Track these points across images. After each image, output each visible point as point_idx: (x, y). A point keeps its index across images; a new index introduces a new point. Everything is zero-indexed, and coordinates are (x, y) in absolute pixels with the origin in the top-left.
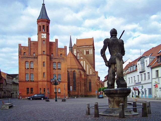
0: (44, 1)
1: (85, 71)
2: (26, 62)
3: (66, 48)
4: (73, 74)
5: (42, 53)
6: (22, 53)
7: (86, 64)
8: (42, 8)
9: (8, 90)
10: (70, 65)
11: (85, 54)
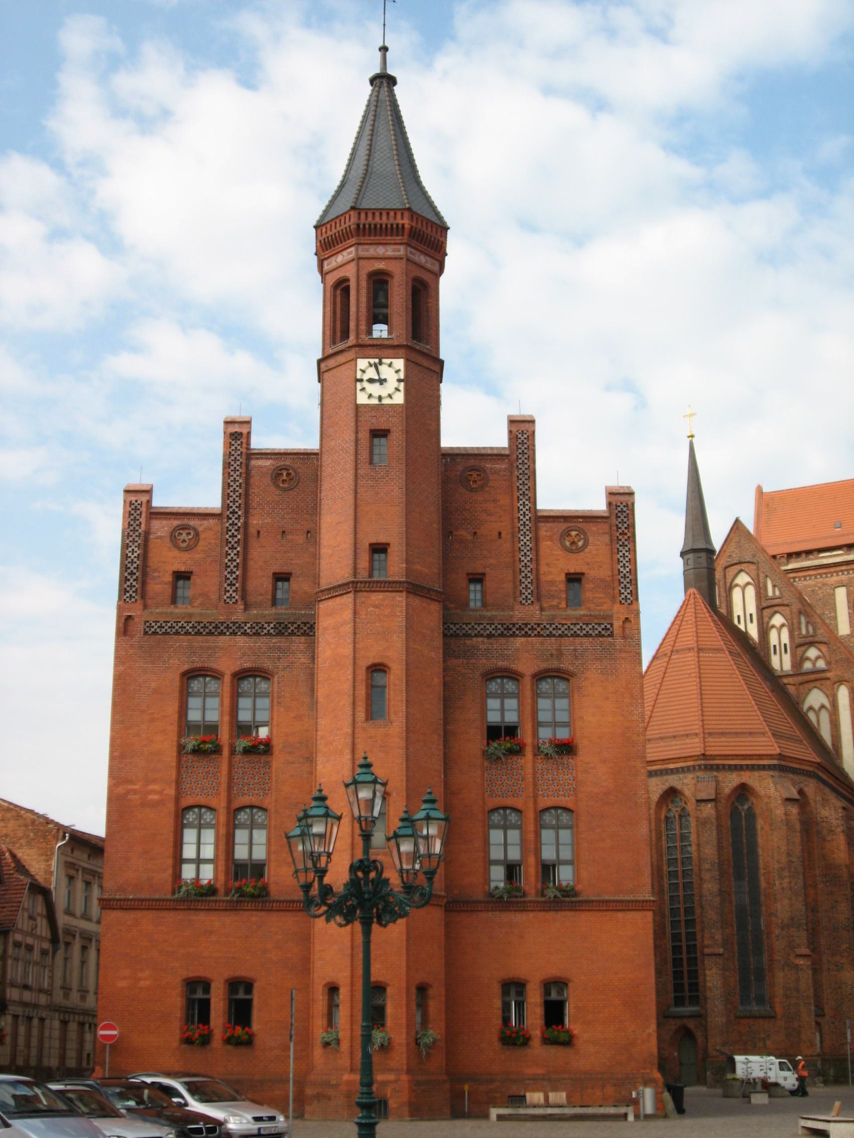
0: (384, 49)
2: (190, 675)
3: (621, 505)
4: (736, 830)
5: (364, 563)
6: (160, 585)
8: (367, 112)
10: (697, 728)
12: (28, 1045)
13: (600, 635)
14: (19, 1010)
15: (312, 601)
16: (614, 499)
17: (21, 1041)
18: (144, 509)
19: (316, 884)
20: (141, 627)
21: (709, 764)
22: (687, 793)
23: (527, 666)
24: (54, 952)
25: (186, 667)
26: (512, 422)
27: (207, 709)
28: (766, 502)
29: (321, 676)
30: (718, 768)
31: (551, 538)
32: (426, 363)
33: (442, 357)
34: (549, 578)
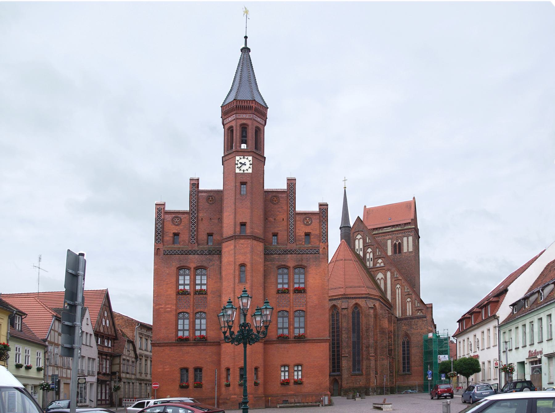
1: (389, 306)
2: (180, 268)
3: (324, 208)
7: (395, 281)
9: (143, 377)
11: (390, 253)
14: (126, 381)
15: (220, 243)
16: (322, 207)
17: (127, 390)
18: (162, 211)
19: (228, 331)
20: (162, 252)
21: (345, 297)
22: (339, 306)
23: (291, 264)
27: (185, 281)
28: (367, 212)
29: (223, 268)
31: (300, 221)
34: (299, 234)
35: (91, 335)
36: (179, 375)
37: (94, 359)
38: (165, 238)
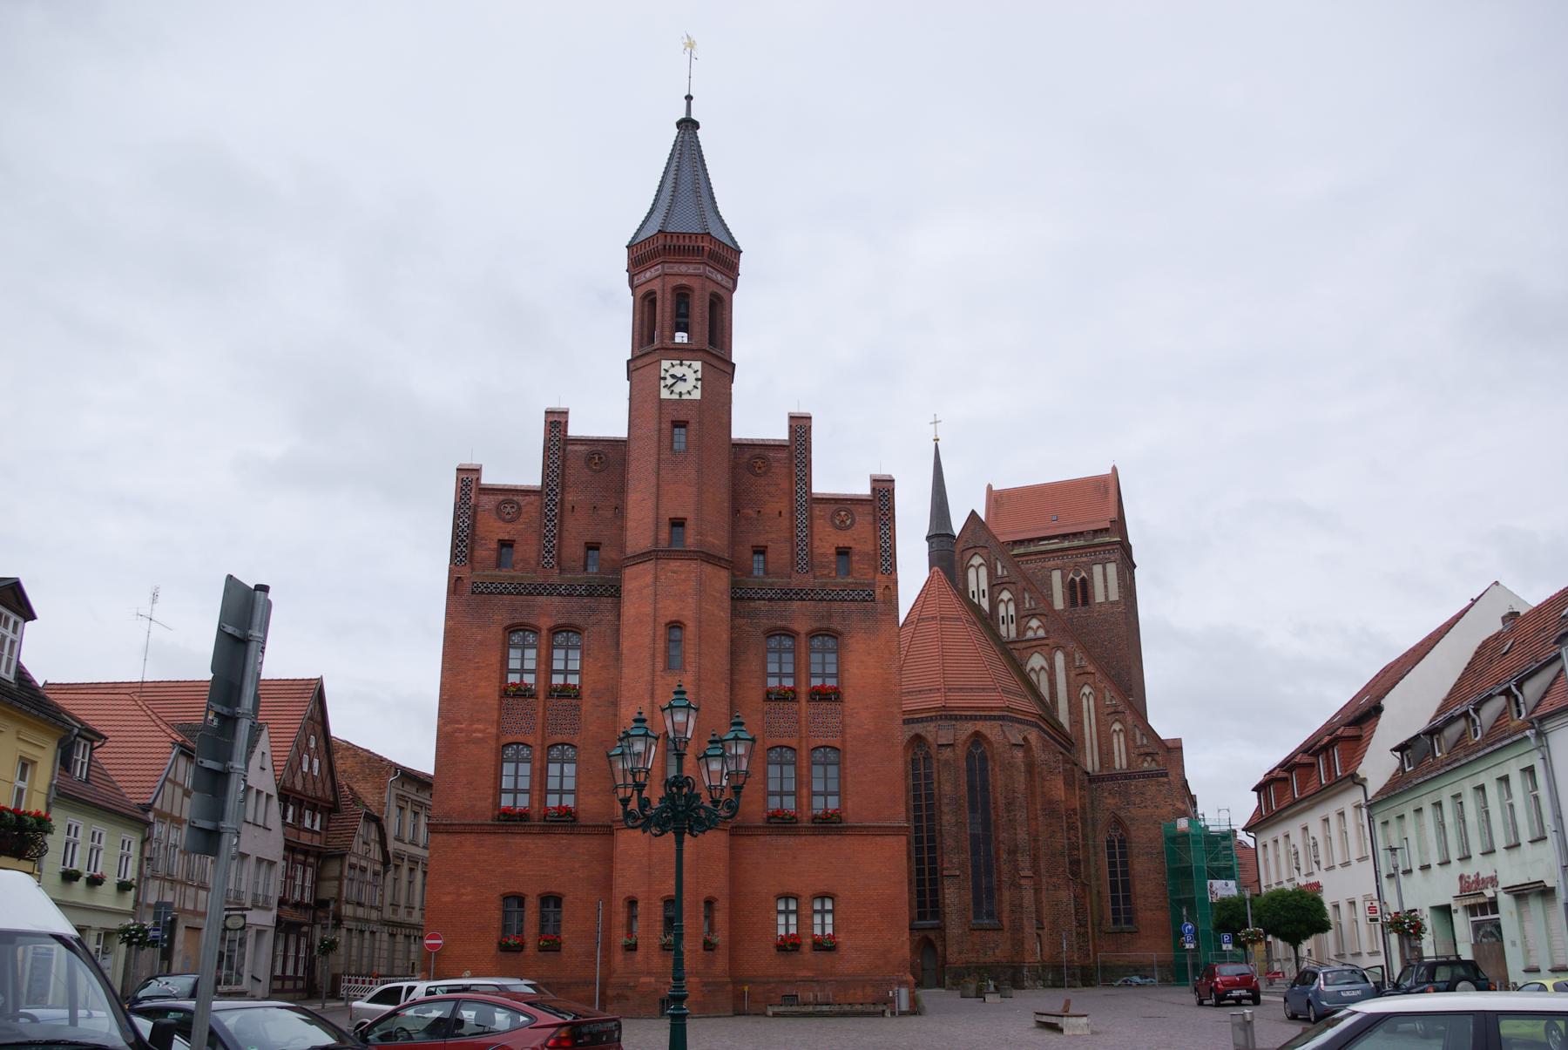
0: (689, 98)
1: (1066, 742)
2: (512, 629)
3: (883, 490)
5: (664, 533)
7: (1077, 677)
9: (402, 915)
11: (1059, 603)
12: (361, 956)
13: (864, 600)
14: (353, 925)
15: (618, 568)
17: (354, 952)
22: (930, 739)
23: (802, 626)
24: (385, 873)
25: (509, 622)
26: (792, 418)
29: (625, 631)
30: (956, 718)
32: (722, 366)
33: (734, 360)
35: (269, 796)
36: (498, 915)
37: (271, 863)
38: (476, 553)
